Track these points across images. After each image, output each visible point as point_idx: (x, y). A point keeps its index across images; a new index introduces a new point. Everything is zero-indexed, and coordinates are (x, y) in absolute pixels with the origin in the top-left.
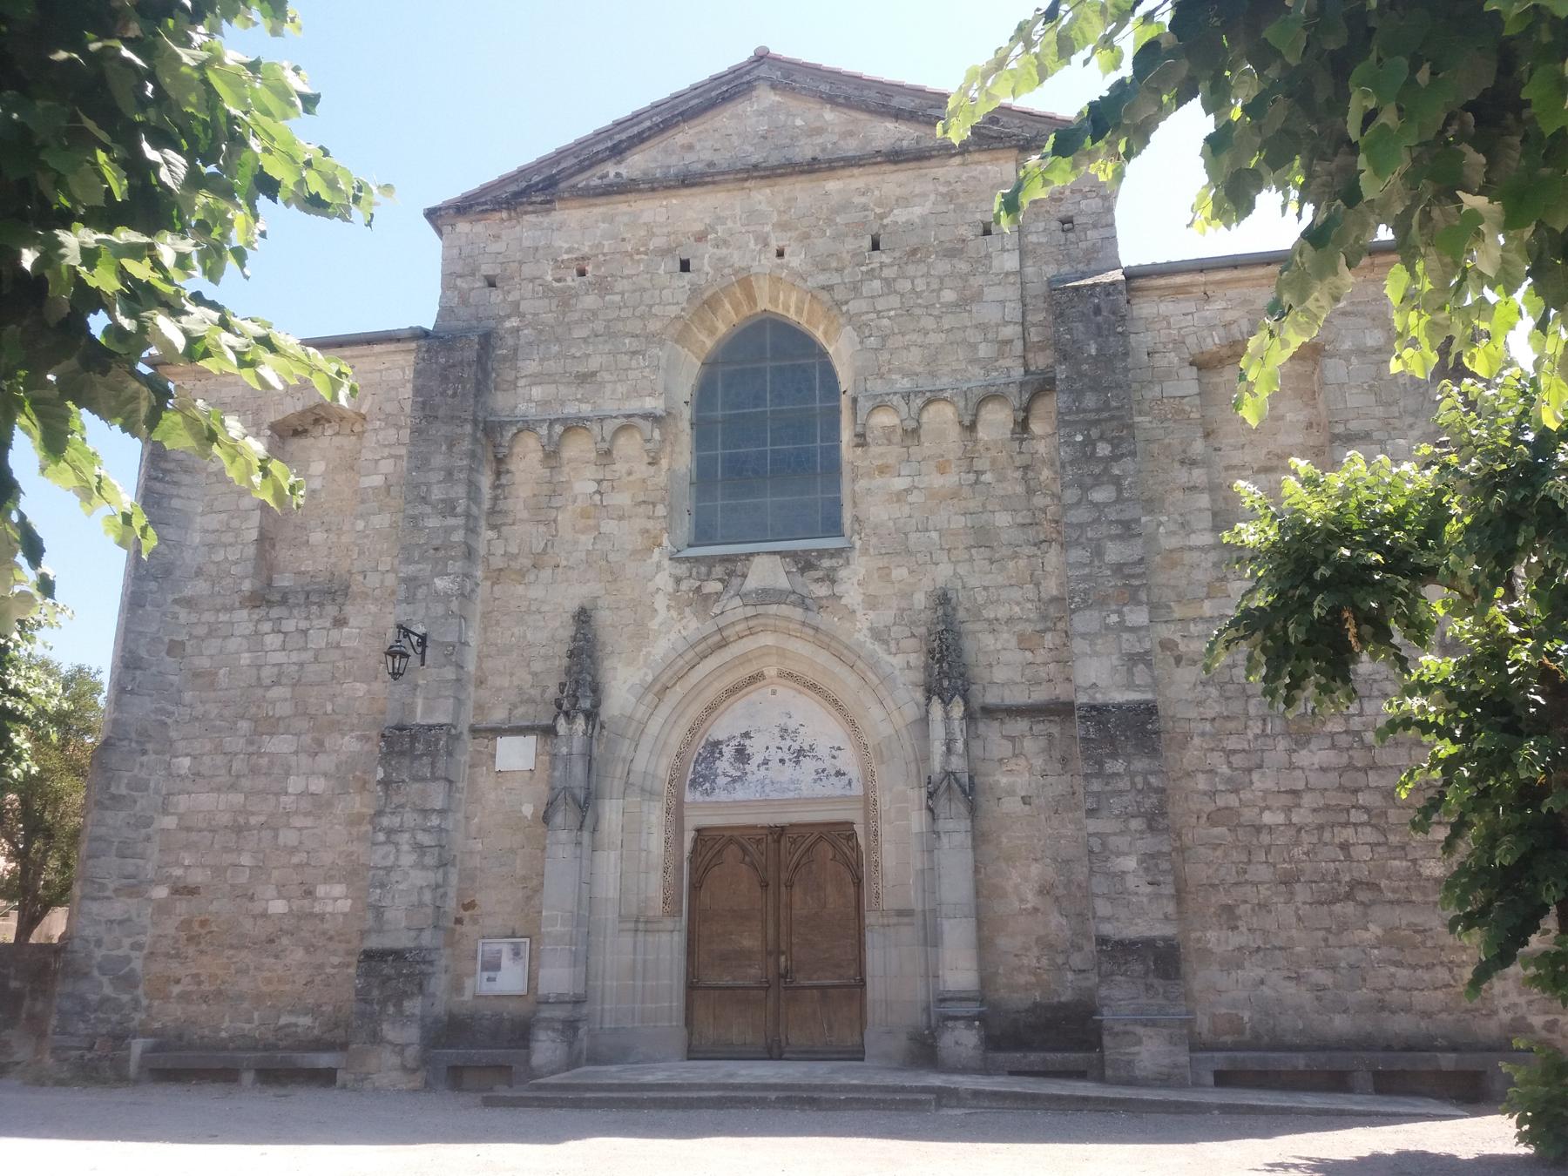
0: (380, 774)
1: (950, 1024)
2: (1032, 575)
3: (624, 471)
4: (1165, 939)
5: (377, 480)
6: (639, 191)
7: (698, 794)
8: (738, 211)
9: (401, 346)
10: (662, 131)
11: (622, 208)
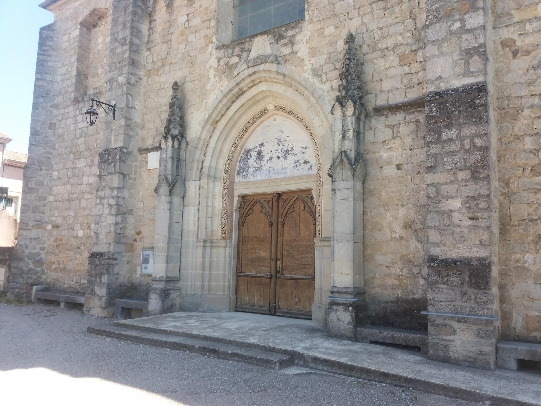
1: (335, 307)
2: (411, 13)
3: (198, 6)
4: (479, 260)
7: (241, 178)
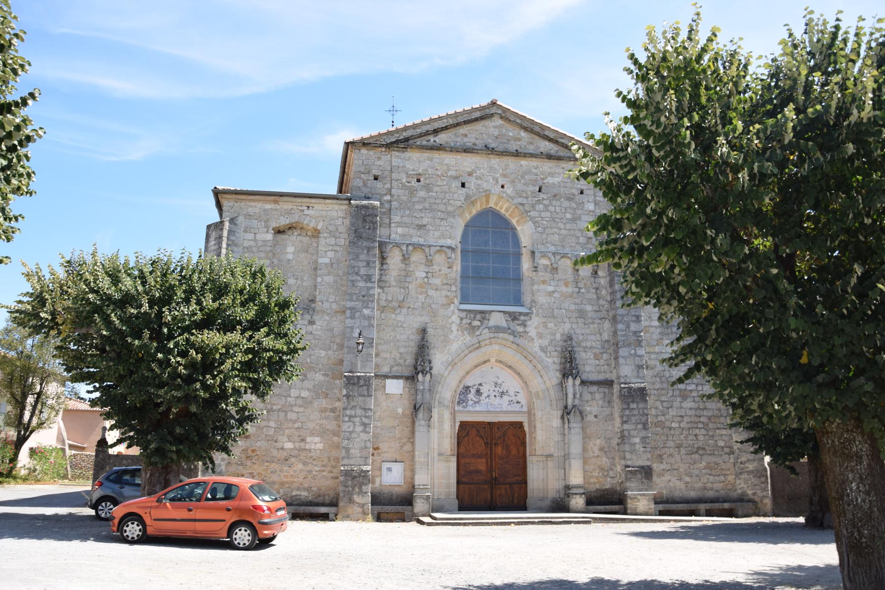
0: (344, 392)
5: (327, 260)
6: (446, 151)
8: (486, 166)
9: (339, 202)
10: (455, 126)
11: (436, 155)
